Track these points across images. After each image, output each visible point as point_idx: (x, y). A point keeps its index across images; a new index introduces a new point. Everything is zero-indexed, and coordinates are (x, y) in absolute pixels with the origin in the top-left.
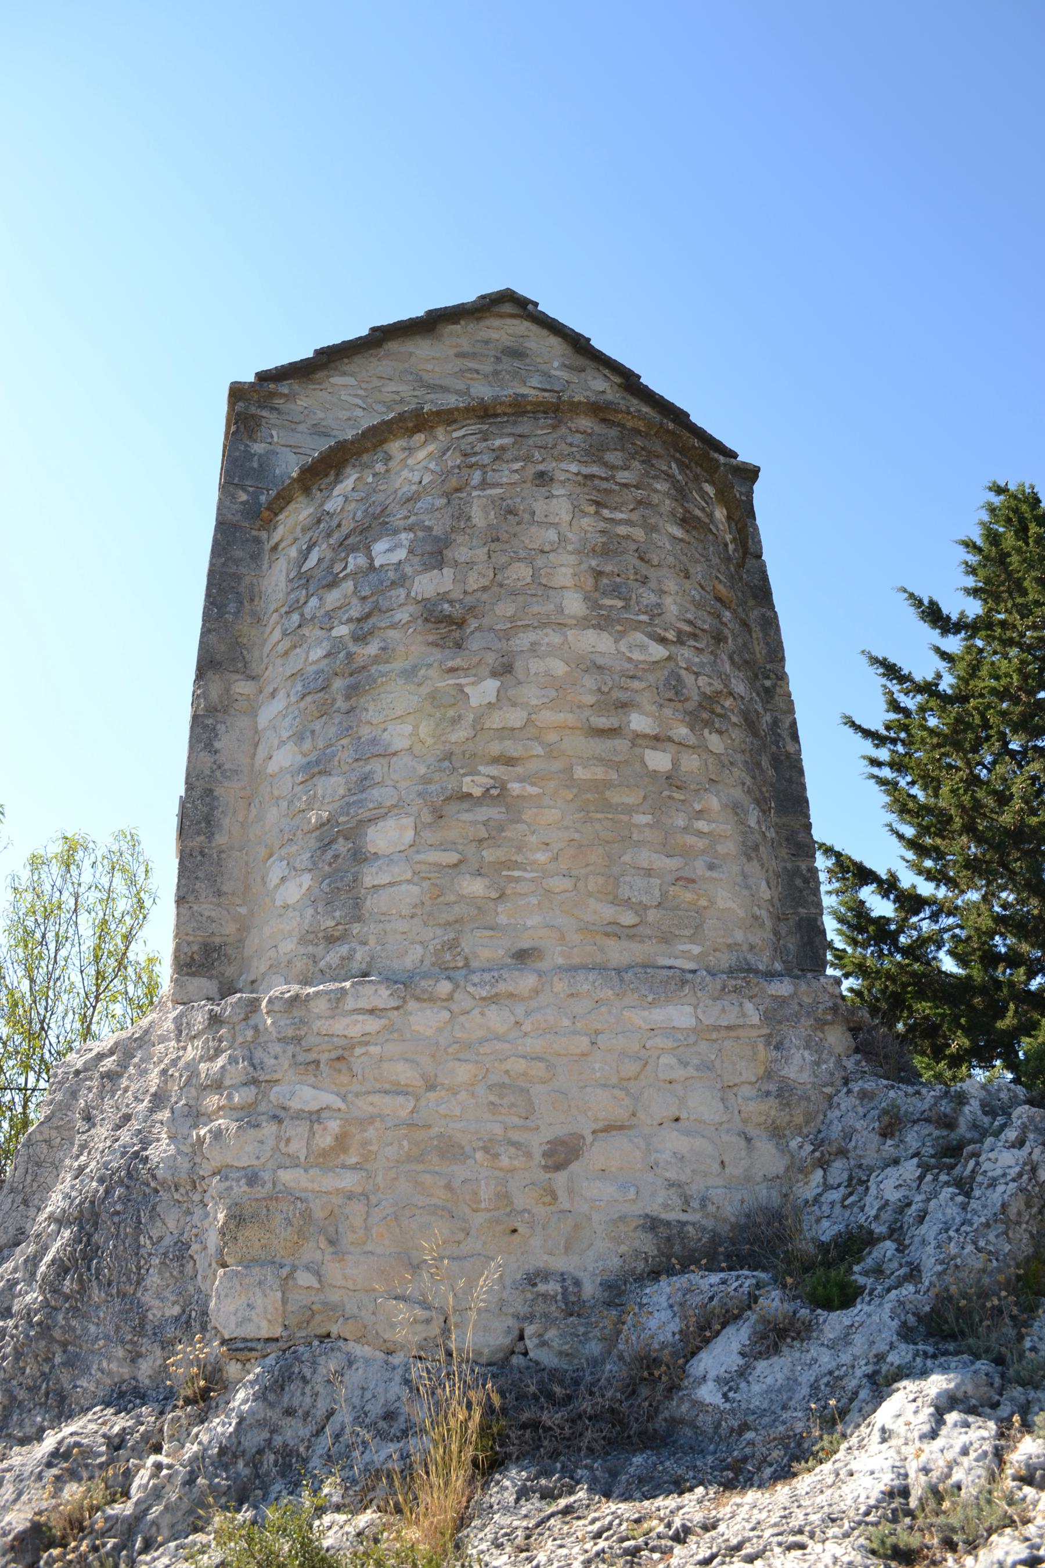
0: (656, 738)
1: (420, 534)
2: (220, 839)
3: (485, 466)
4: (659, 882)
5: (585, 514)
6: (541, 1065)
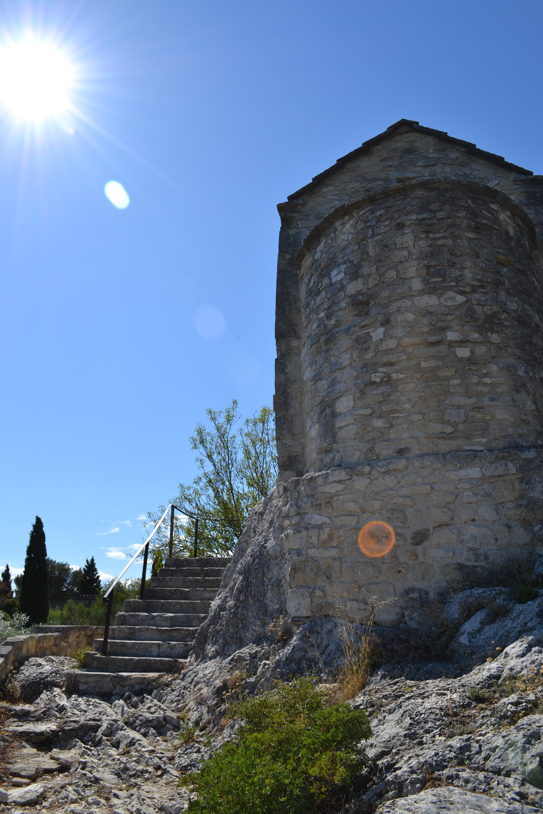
0: (462, 342)
1: (349, 264)
2: (291, 411)
3: (373, 226)
4: (464, 410)
5: (420, 239)
6: (410, 500)
